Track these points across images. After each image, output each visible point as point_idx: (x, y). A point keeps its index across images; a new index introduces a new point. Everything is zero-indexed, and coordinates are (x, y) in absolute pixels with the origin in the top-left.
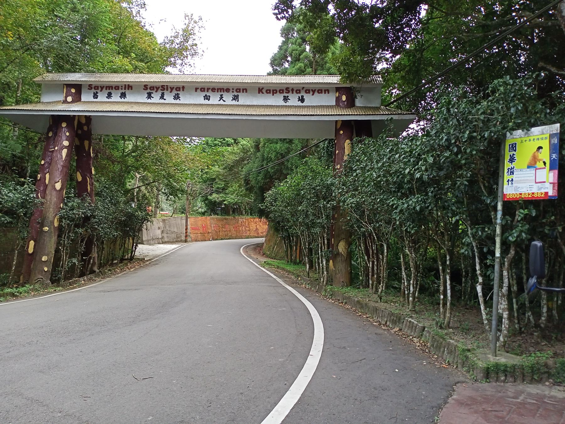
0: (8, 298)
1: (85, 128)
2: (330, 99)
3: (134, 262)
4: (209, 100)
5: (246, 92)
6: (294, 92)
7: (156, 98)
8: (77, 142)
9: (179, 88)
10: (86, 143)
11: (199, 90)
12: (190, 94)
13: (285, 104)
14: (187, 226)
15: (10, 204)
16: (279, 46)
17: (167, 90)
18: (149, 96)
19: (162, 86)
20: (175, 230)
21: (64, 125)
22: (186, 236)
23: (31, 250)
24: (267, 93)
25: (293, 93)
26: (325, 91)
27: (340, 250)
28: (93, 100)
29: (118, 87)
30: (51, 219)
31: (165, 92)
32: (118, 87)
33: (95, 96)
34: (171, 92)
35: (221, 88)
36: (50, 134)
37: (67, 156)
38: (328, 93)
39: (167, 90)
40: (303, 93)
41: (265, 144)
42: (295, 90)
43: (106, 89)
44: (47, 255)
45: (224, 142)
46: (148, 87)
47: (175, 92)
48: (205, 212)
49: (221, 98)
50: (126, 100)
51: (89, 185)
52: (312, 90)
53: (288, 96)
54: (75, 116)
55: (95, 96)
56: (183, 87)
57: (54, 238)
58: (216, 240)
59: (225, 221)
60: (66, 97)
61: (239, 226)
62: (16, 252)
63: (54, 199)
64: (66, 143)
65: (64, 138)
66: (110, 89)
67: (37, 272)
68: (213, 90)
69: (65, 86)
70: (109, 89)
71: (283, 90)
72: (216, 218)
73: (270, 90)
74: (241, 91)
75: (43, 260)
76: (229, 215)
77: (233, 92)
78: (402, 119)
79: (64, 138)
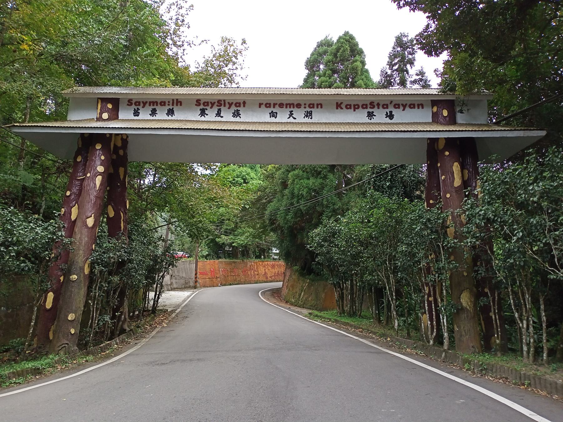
0: (29, 377)
1: (121, 152)
2: (425, 115)
3: (159, 315)
4: (276, 118)
5: (321, 107)
6: (381, 107)
7: (211, 116)
8: (112, 171)
9: (240, 103)
10: (121, 170)
11: (263, 106)
12: (253, 111)
13: (370, 121)
14: (196, 270)
15: (33, 245)
16: (305, 79)
17: (225, 106)
18: (203, 113)
19: (219, 101)
20: (184, 275)
21: (98, 147)
22: (196, 282)
23: (49, 304)
24: (347, 108)
25: (378, 108)
26: (418, 105)
27: (464, 304)
28: (132, 117)
29: (165, 102)
30: (81, 265)
31: (222, 108)
32: (165, 102)
33: (136, 113)
34: (229, 108)
35: (291, 102)
36: (79, 159)
37: (101, 185)
38: (423, 108)
39: (225, 106)
40: (391, 108)
41: (294, 181)
42: (381, 104)
43: (150, 105)
44: (75, 312)
45: (233, 182)
46: (202, 102)
47: (234, 108)
48: (208, 255)
49: (291, 114)
50: (174, 118)
51: (122, 222)
52: (402, 105)
53: (373, 112)
54: (111, 134)
55: (136, 113)
56: (244, 103)
57: (83, 290)
58: (225, 285)
59: (233, 264)
60: (101, 114)
61: (247, 270)
62: (36, 308)
63: (85, 239)
64: (101, 169)
65: (98, 162)
66: (154, 104)
67: (61, 335)
68: (281, 105)
69: (100, 101)
70: (153, 105)
71: (366, 105)
72: (225, 262)
73: (350, 105)
74: (315, 106)
75: (69, 318)
76: (237, 258)
77: (305, 108)
78: (528, 137)
79: (98, 162)
